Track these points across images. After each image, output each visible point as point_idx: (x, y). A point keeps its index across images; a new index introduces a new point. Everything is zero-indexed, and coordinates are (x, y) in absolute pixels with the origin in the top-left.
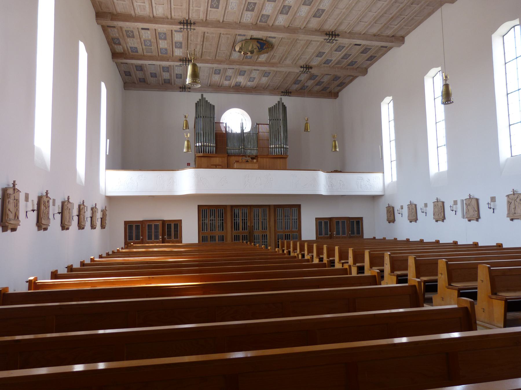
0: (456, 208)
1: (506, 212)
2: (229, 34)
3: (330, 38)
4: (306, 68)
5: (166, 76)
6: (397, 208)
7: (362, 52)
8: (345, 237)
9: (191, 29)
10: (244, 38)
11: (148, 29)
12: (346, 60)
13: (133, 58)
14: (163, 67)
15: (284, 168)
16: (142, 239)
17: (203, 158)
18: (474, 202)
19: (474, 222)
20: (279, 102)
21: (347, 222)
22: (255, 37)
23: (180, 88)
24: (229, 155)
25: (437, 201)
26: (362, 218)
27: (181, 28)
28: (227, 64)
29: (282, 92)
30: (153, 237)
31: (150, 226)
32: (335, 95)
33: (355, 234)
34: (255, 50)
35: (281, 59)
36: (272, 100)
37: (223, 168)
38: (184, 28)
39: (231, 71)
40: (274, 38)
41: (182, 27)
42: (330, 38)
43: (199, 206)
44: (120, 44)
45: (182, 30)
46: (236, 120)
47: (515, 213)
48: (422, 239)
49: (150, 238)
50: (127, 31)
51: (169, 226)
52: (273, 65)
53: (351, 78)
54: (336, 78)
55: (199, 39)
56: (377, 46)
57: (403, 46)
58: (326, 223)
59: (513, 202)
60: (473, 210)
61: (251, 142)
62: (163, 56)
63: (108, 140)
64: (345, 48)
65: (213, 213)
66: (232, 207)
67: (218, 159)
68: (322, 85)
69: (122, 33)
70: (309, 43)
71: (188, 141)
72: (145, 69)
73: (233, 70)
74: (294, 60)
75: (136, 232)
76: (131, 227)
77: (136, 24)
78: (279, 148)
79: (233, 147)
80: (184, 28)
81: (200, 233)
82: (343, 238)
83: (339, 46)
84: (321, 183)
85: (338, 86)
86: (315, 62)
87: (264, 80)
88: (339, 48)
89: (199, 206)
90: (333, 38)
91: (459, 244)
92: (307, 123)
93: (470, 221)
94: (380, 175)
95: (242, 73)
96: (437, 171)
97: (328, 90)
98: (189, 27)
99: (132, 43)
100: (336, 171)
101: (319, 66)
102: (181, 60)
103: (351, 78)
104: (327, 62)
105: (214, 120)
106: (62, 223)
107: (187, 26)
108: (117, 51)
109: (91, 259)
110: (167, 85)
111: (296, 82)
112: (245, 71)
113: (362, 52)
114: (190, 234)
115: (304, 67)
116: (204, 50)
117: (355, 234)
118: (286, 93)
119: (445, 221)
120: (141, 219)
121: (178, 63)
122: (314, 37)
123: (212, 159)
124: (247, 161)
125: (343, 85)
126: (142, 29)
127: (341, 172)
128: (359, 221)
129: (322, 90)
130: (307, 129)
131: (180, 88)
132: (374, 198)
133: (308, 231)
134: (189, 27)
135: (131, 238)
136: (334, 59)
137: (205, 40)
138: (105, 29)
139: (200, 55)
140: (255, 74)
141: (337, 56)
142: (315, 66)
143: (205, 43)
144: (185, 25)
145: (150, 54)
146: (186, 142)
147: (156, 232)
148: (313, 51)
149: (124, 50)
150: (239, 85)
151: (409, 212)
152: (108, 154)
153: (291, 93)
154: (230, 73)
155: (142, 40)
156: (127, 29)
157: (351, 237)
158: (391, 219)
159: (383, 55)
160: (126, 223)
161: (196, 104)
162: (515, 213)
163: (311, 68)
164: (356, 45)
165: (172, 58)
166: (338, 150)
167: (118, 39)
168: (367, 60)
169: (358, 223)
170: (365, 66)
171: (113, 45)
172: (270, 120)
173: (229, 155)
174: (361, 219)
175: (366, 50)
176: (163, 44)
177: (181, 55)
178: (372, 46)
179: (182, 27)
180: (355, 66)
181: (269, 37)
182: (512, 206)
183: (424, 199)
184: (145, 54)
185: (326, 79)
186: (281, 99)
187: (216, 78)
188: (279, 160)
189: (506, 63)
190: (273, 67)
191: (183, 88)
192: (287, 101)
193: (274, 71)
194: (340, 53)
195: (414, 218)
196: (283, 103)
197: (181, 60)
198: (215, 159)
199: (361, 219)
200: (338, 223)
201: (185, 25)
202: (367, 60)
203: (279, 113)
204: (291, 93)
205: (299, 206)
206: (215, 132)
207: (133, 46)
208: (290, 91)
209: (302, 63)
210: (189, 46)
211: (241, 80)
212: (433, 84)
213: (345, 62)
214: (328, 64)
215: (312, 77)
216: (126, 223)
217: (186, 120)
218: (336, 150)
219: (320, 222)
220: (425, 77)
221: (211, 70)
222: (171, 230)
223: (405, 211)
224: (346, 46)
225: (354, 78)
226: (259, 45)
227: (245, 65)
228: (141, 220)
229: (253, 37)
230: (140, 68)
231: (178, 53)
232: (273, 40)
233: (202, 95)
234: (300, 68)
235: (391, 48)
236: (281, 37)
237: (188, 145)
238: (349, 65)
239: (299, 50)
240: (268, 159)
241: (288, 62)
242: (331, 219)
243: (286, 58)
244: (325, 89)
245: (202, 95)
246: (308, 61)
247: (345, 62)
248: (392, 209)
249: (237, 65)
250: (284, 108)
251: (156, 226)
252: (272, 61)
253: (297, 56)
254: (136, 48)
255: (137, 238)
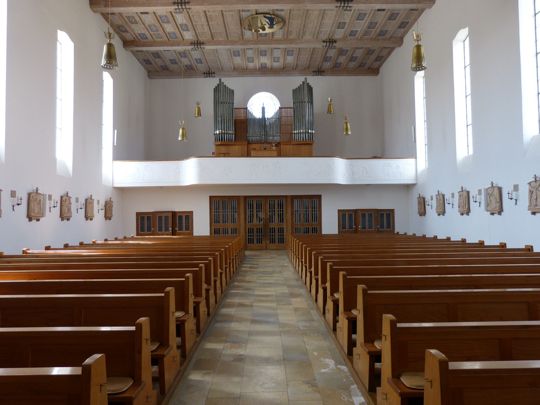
0: (481, 199)
1: (527, 204)
2: (232, 11)
3: (342, 5)
4: (329, 42)
5: (185, 61)
6: (428, 198)
7: (390, 19)
8: (372, 232)
9: (186, 9)
10: (249, 13)
11: (147, 13)
12: (374, 30)
13: (144, 45)
14: (180, 53)
15: (310, 155)
16: (153, 231)
17: (221, 147)
18: (496, 192)
19: (496, 215)
20: (303, 82)
21: (375, 214)
22: (260, 11)
23: (204, 73)
24: (249, 143)
25: (462, 191)
26: (393, 210)
27: (176, 9)
28: (241, 44)
29: (314, 72)
30: (164, 229)
31: (160, 218)
32: (374, 71)
33: (385, 229)
34: (265, 26)
35: (299, 35)
36: (297, 81)
37: (242, 156)
38: (179, 9)
39: (250, 51)
40: (282, 10)
41: (177, 7)
42: (342, 5)
43: (210, 197)
44: (127, 32)
45: (178, 10)
46: (264, 105)
47: (536, 205)
48: (449, 236)
49: (160, 230)
50: (128, 17)
51: (180, 217)
52: (291, 41)
53: (388, 50)
54: (369, 52)
55: (203, 19)
56: (405, 10)
57: (435, 6)
58: (350, 216)
59: (535, 191)
60: (496, 202)
61: (273, 128)
62: (171, 40)
63: (116, 131)
64: (367, 16)
65: (223, 203)
66: (245, 197)
67: (237, 146)
68: (357, 61)
69: (124, 19)
70: (323, 13)
71: (183, 129)
72: (162, 55)
73: (252, 50)
74: (314, 34)
75: (146, 222)
76: (142, 218)
77: (130, 8)
78: (303, 133)
79: (253, 134)
80: (340, 6)
81: (212, 225)
82: (369, 232)
83: (360, 14)
84: (339, 170)
85: (376, 60)
86: (339, 34)
87: (290, 59)
88: (361, 16)
89: (210, 197)
90: (346, 5)
91: (467, 242)
92: (330, 104)
93: (492, 214)
94: (412, 161)
95: (263, 53)
96: (467, 155)
97: (367, 66)
98: (184, 7)
99: (138, 29)
100: (375, 157)
101: (344, 38)
102: (192, 43)
103: (388, 50)
104: (353, 33)
105: (233, 105)
106: (28, 214)
107: (181, 6)
108: (127, 38)
109: (23, 251)
110: (190, 71)
111: (326, 59)
112: (266, 51)
113: (390, 19)
114: (202, 227)
115: (327, 42)
116: (213, 31)
117: (385, 229)
118: (319, 72)
119: (502, 213)
120: (152, 211)
121: (190, 48)
122: (323, 5)
123: (231, 147)
124: (265, 149)
125: (381, 59)
126: (142, 13)
127: (380, 158)
128: (389, 214)
129: (360, 66)
130: (331, 112)
131: (204, 73)
132: (408, 187)
133: (330, 225)
134: (184, 7)
135: (143, 230)
136: (359, 30)
137: (209, 20)
138: (105, 16)
139: (210, 36)
140: (277, 54)
141: (361, 26)
142: (340, 39)
143: (210, 23)
144: (180, 5)
145: (161, 39)
146: (208, 129)
147: (167, 224)
148: (331, 22)
149: (134, 38)
150: (266, 67)
151: (437, 203)
152: (115, 144)
153: (323, 72)
154: (250, 53)
155: (146, 25)
156: (128, 15)
157: (379, 232)
158: (423, 213)
159: (416, 20)
160: (138, 214)
161: (214, 89)
162: (536, 205)
163: (335, 42)
164: (379, 10)
165: (183, 42)
166: (349, 133)
167: (123, 26)
168: (400, 27)
169: (388, 216)
170: (399, 35)
171: (121, 33)
172: (294, 103)
173: (249, 143)
174: (392, 211)
175: (393, 16)
176: (169, 28)
177: (192, 38)
178: (399, 10)
179: (177, 7)
180: (387, 36)
181: (277, 10)
182: (534, 197)
183: (451, 190)
184: (155, 40)
185: (359, 54)
186: (306, 79)
187: (238, 61)
188: (303, 146)
189: (535, 14)
190: (291, 43)
191: (207, 73)
192: (314, 81)
193: (297, 48)
194: (364, 21)
195: (466, 210)
196: (308, 84)
197: (192, 43)
198: (234, 146)
199: (392, 211)
200: (364, 216)
201: (180, 5)
202: (400, 27)
203: (303, 96)
204: (323, 72)
205: (320, 197)
206: (234, 118)
207: (140, 32)
208: (322, 70)
209: (324, 36)
210: (196, 28)
211: (265, 60)
212: (461, 49)
213: (373, 33)
214: (354, 36)
215: (341, 52)
216: (138, 214)
217: (198, 107)
218: (347, 134)
219: (342, 214)
220: (454, 42)
221: (229, 52)
222: (180, 221)
223: (434, 203)
224: (368, 12)
225: (392, 49)
226: (268, 21)
227: (261, 44)
228: (152, 211)
229: (258, 12)
230: (157, 55)
231: (188, 36)
232: (282, 14)
233: (220, 80)
234: (322, 43)
235: (423, 10)
236: (289, 8)
237: (183, 133)
238: (379, 35)
239: (316, 22)
240: (291, 146)
241: (308, 37)
242: (356, 211)
243: (304, 33)
244: (361, 65)
245: (220, 80)
246: (329, 34)
247: (373, 33)
248: (422, 200)
249: (252, 44)
250: (310, 89)
251: (167, 218)
252: (291, 37)
253: (316, 29)
254: (144, 34)
255: (149, 230)
